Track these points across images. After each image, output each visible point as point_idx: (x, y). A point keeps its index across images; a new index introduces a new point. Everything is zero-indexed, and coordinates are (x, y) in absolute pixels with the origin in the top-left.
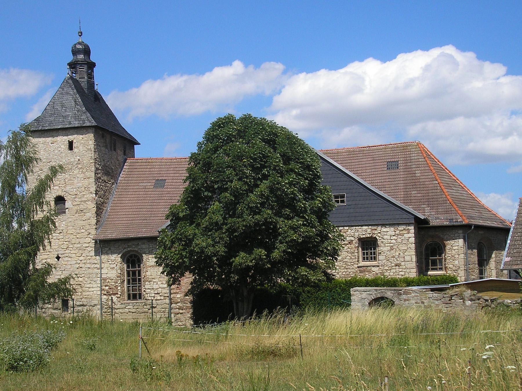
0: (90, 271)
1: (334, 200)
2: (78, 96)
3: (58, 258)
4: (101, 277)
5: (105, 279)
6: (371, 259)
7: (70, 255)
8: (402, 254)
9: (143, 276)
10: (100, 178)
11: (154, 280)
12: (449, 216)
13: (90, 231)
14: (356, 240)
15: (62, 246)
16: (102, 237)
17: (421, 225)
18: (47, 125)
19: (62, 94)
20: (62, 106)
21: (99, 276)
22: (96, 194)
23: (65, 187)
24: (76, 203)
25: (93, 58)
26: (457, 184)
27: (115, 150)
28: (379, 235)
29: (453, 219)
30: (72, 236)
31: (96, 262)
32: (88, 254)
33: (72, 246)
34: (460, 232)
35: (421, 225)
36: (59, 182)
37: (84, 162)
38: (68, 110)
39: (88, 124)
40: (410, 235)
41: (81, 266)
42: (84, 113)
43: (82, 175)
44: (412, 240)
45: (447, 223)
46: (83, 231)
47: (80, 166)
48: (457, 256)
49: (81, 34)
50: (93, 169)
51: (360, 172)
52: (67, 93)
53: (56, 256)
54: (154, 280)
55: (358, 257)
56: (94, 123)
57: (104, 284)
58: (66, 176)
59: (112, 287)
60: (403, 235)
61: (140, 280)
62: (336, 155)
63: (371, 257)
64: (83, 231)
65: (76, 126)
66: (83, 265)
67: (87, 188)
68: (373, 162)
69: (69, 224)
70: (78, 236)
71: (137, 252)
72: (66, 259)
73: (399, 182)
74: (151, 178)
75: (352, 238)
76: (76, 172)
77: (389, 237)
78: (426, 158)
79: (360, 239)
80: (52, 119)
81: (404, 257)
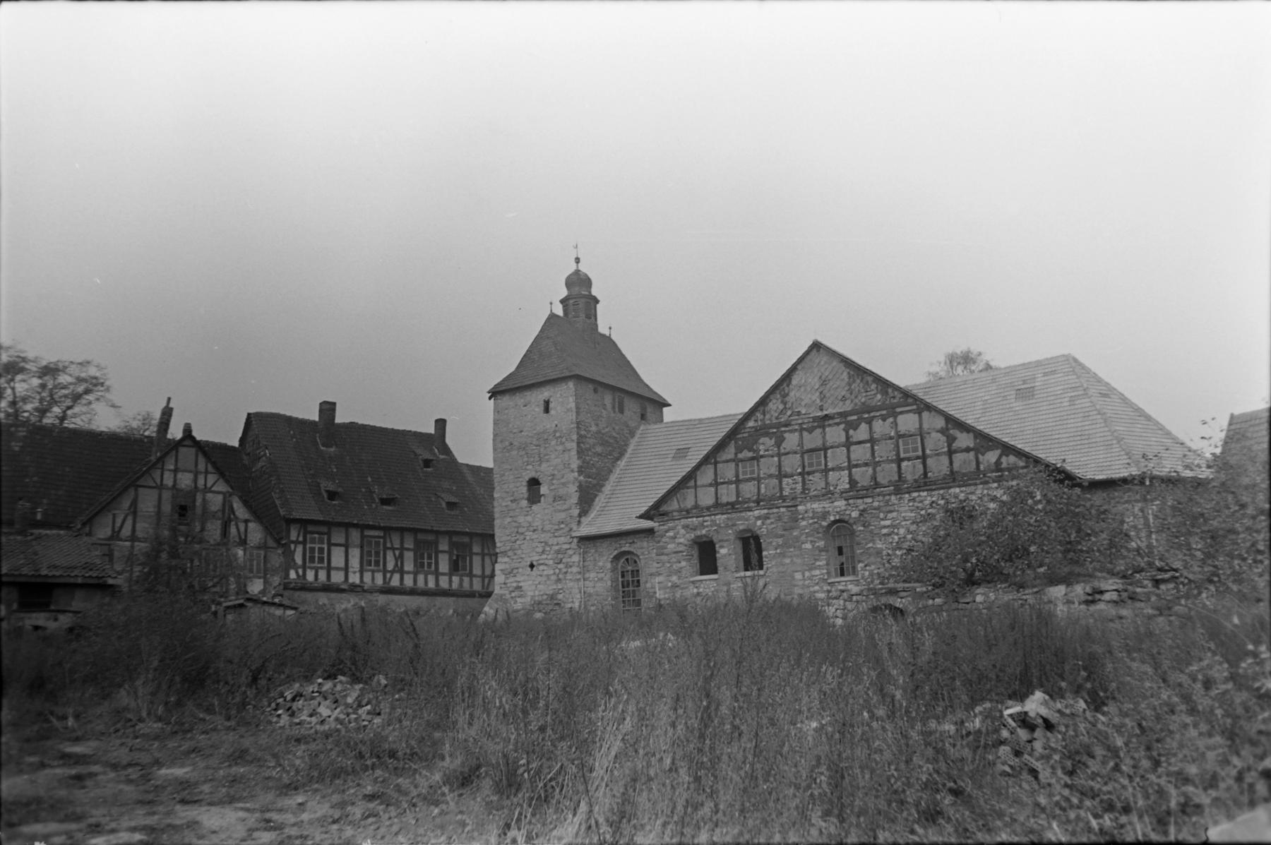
25: (595, 292)
43: (560, 448)
49: (578, 260)
50: (575, 437)
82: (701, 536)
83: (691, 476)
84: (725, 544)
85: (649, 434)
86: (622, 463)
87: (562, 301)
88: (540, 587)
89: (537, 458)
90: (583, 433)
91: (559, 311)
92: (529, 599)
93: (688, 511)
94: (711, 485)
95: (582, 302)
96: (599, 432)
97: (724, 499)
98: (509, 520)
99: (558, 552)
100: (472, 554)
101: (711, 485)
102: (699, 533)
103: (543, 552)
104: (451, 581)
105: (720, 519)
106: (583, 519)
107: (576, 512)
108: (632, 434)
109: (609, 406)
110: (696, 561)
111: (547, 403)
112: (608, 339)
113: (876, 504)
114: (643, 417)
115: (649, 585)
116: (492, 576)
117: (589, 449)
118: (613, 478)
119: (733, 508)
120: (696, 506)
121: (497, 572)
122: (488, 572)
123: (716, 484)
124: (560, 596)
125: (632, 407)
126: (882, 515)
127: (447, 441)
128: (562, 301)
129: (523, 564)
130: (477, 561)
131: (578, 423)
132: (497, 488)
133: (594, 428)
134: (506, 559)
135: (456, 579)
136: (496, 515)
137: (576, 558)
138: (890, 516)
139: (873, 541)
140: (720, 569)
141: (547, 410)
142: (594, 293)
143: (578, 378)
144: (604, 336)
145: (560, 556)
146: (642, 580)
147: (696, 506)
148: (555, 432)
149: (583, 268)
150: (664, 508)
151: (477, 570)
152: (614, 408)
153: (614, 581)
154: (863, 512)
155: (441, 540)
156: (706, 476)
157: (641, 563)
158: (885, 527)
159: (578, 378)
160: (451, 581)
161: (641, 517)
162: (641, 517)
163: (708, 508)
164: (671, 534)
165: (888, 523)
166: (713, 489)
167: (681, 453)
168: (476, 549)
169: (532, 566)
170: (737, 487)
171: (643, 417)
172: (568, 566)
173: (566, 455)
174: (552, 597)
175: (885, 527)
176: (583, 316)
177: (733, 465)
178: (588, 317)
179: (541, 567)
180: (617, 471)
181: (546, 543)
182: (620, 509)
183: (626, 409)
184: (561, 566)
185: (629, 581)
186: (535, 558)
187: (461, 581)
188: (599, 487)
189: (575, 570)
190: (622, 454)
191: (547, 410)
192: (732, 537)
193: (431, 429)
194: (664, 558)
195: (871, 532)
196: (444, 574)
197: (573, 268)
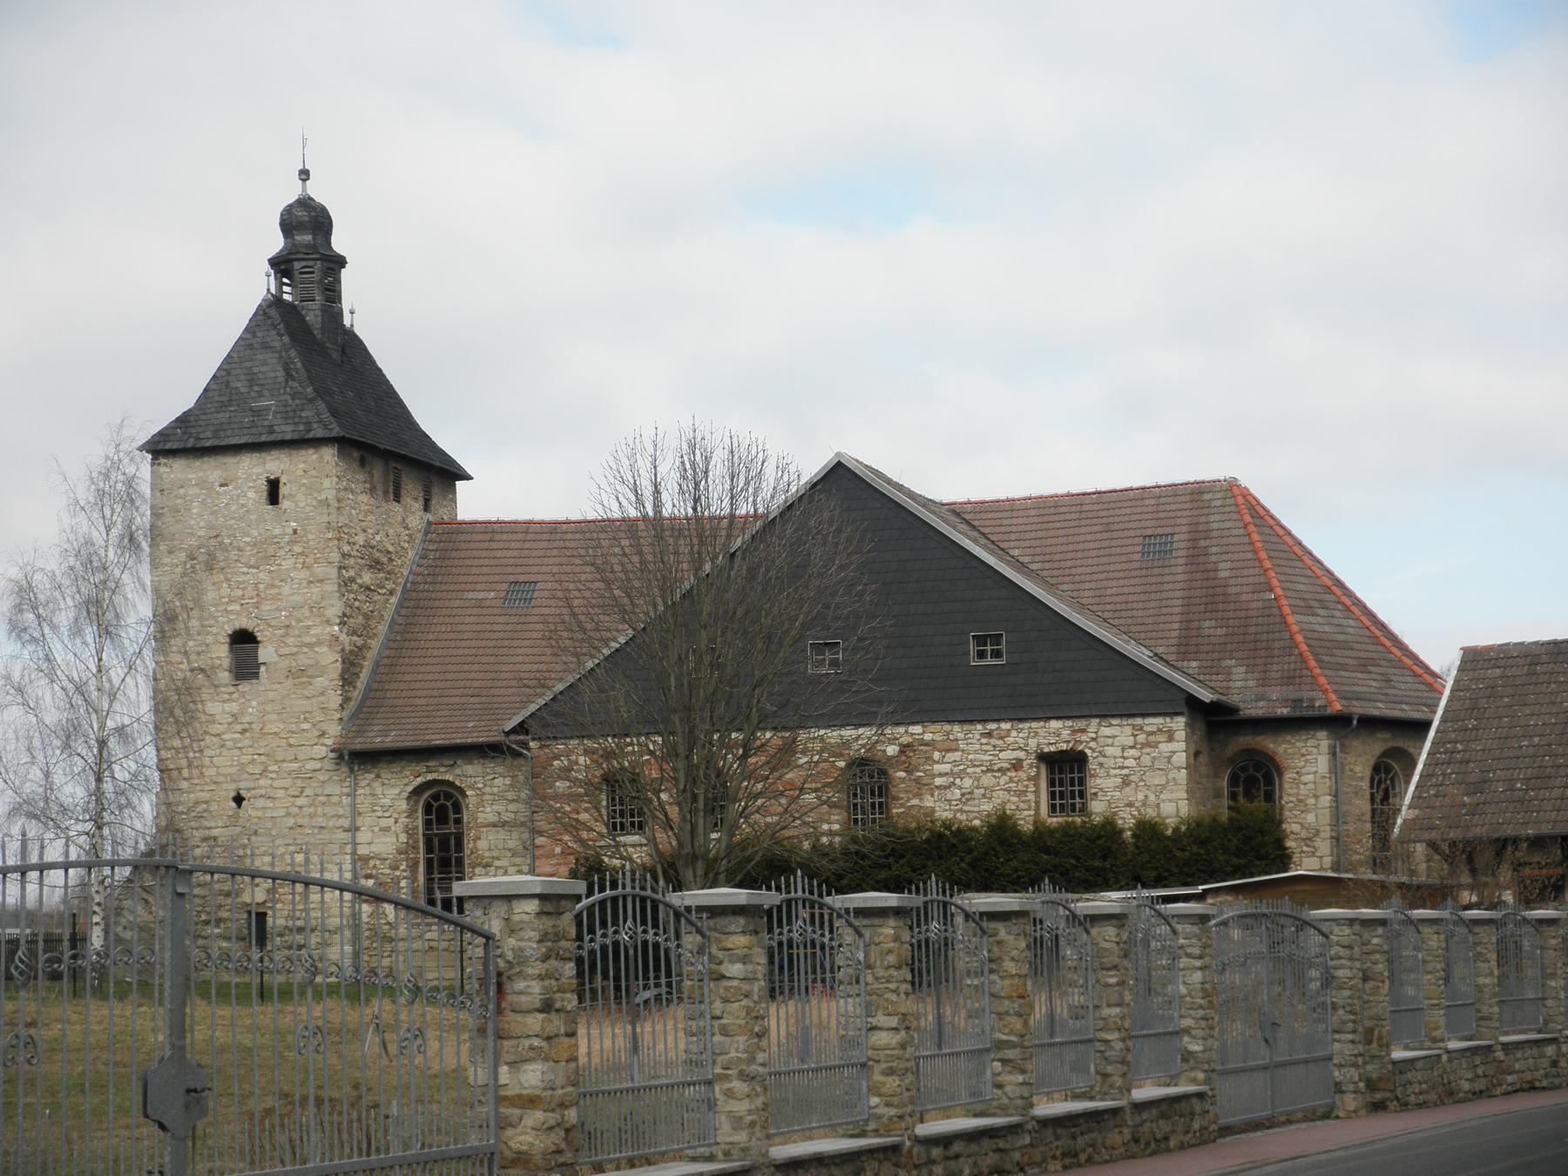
0: (325, 836)
1: (972, 647)
2: (293, 353)
3: (239, 800)
4: (354, 853)
5: (365, 859)
6: (622, 828)
7: (271, 793)
8: (1152, 797)
9: (467, 852)
10: (352, 580)
11: (498, 863)
12: (1291, 692)
13: (324, 726)
14: (1032, 760)
15: (250, 769)
16: (359, 744)
17: (1214, 720)
18: (209, 434)
19: (251, 346)
20: (252, 382)
21: (348, 849)
22: (343, 623)
24: (284, 651)
25: (339, 243)
26: (1332, 598)
27: (397, 498)
28: (1093, 744)
29: (1301, 701)
30: (277, 742)
31: (341, 812)
32: (319, 791)
33: (275, 768)
34: (1322, 734)
35: (1214, 720)
36: (240, 593)
37: (311, 537)
38: (266, 393)
39: (319, 432)
40: (1174, 746)
41: (300, 822)
42: (311, 401)
43: (304, 574)
44: (1181, 758)
45: (1285, 711)
46: (306, 726)
47: (297, 549)
48: (1312, 801)
49: (304, 174)
50: (335, 556)
51: (1069, 564)
52: (265, 346)
53: (233, 794)
54: (498, 863)
55: (1037, 803)
56: (336, 431)
57: (364, 872)
58: (261, 575)
59: (383, 879)
60: (1155, 745)
61: (460, 862)
62: (1008, 514)
63: (632, 824)
64: (306, 726)
65: (288, 437)
66: (304, 821)
67: (316, 609)
68: (1105, 535)
69: (269, 708)
70: (292, 741)
71: (452, 784)
72: (261, 803)
73: (1170, 594)
74: (497, 578)
75: (1022, 755)
76: (287, 564)
77: (1118, 752)
78: (1252, 528)
79: (1043, 757)
80: (223, 417)
81: (1158, 806)
113: (928, 737)
126: (936, 755)
138: (950, 756)
139: (919, 795)
149: (318, 192)
154: (905, 748)
158: (941, 775)
165: (946, 768)
175: (941, 775)
195: (918, 780)
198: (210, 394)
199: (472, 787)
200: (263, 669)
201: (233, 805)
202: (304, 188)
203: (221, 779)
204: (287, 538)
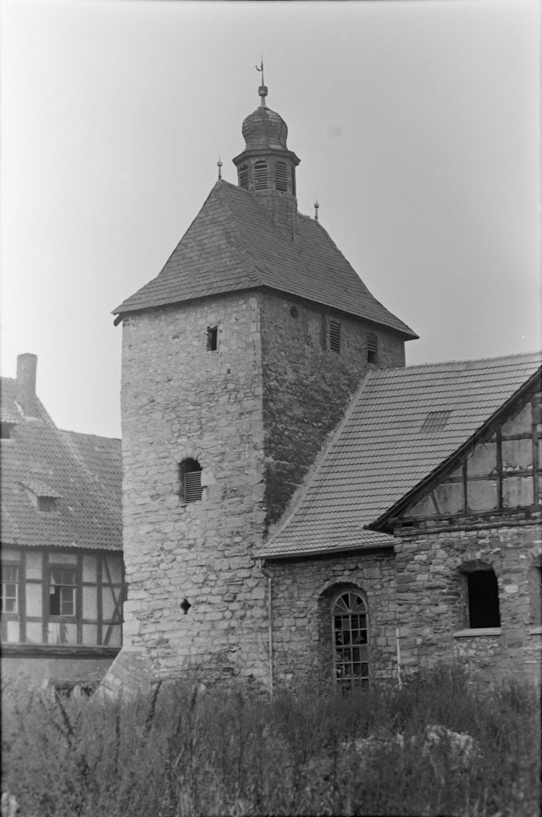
23: (200, 437)
24: (222, 474)
36: (187, 427)
43: (234, 409)
46: (237, 539)
47: (231, 386)
49: (263, 91)
50: (260, 391)
52: (214, 222)
53: (181, 601)
70: (227, 553)
82: (471, 563)
83: (456, 462)
84: (514, 577)
85: (379, 381)
86: (336, 436)
87: (236, 161)
88: (200, 640)
89: (196, 426)
90: (274, 383)
91: (232, 176)
92: (181, 659)
93: (451, 520)
94: (490, 477)
95: (270, 164)
96: (299, 383)
97: (513, 502)
98: (149, 528)
99: (230, 582)
100: (80, 585)
101: (490, 477)
102: (469, 556)
103: (205, 583)
104: (45, 631)
105: (506, 534)
106: (272, 528)
107: (261, 516)
108: (353, 386)
109: (316, 339)
110: (463, 603)
111: (213, 333)
112: (313, 227)
114: (371, 357)
115: (381, 641)
116: (118, 619)
117: (282, 412)
118: (321, 459)
119: (528, 516)
120: (466, 512)
121: (127, 616)
122: (107, 615)
123: (499, 475)
124: (232, 657)
125: (352, 340)
127: (39, 392)
128: (236, 161)
129: (172, 601)
130: (89, 596)
131: (265, 367)
132: (128, 475)
133: (291, 377)
134: (142, 594)
135: (54, 628)
136: (127, 521)
137: (259, 593)
140: (505, 618)
141: (213, 345)
142: (290, 148)
143: (266, 292)
144: (306, 219)
145: (233, 589)
146: (371, 631)
147: (466, 512)
148: (226, 381)
149: (272, 103)
150: (411, 513)
151: (89, 612)
152: (323, 342)
153: (324, 634)
155: (29, 562)
156: (484, 461)
157: (369, 604)
159: (266, 292)
160: (45, 631)
161: (373, 527)
162: (373, 527)
163: (486, 516)
164: (422, 557)
166: (494, 484)
167: (436, 420)
168: (89, 575)
169: (186, 606)
170: (535, 482)
171: (371, 357)
172: (247, 606)
173: (246, 419)
174: (220, 658)
176: (272, 185)
177: (529, 444)
178: (281, 188)
179: (202, 608)
180: (328, 448)
181: (210, 567)
182: (337, 511)
183: (343, 343)
184: (234, 606)
185: (347, 630)
186: (191, 592)
187: (63, 631)
188: (298, 474)
189: (258, 612)
190: (336, 420)
191: (213, 345)
192: (525, 566)
193: (10, 371)
194: (410, 596)
196: (33, 620)
197: (255, 104)
198: (170, 264)
199: (372, 588)
200: (204, 492)
201: (182, 611)
202: (263, 102)
203: (172, 589)
204: (222, 378)
